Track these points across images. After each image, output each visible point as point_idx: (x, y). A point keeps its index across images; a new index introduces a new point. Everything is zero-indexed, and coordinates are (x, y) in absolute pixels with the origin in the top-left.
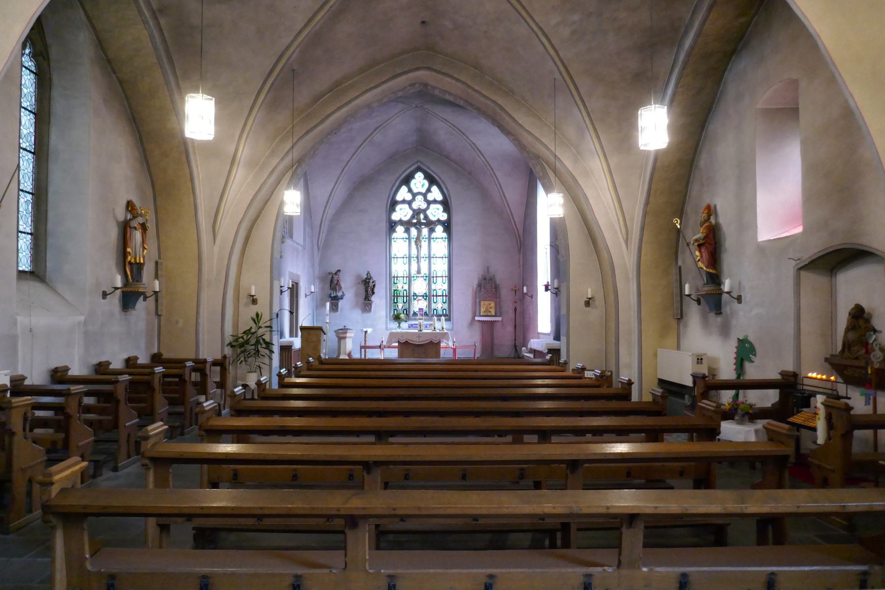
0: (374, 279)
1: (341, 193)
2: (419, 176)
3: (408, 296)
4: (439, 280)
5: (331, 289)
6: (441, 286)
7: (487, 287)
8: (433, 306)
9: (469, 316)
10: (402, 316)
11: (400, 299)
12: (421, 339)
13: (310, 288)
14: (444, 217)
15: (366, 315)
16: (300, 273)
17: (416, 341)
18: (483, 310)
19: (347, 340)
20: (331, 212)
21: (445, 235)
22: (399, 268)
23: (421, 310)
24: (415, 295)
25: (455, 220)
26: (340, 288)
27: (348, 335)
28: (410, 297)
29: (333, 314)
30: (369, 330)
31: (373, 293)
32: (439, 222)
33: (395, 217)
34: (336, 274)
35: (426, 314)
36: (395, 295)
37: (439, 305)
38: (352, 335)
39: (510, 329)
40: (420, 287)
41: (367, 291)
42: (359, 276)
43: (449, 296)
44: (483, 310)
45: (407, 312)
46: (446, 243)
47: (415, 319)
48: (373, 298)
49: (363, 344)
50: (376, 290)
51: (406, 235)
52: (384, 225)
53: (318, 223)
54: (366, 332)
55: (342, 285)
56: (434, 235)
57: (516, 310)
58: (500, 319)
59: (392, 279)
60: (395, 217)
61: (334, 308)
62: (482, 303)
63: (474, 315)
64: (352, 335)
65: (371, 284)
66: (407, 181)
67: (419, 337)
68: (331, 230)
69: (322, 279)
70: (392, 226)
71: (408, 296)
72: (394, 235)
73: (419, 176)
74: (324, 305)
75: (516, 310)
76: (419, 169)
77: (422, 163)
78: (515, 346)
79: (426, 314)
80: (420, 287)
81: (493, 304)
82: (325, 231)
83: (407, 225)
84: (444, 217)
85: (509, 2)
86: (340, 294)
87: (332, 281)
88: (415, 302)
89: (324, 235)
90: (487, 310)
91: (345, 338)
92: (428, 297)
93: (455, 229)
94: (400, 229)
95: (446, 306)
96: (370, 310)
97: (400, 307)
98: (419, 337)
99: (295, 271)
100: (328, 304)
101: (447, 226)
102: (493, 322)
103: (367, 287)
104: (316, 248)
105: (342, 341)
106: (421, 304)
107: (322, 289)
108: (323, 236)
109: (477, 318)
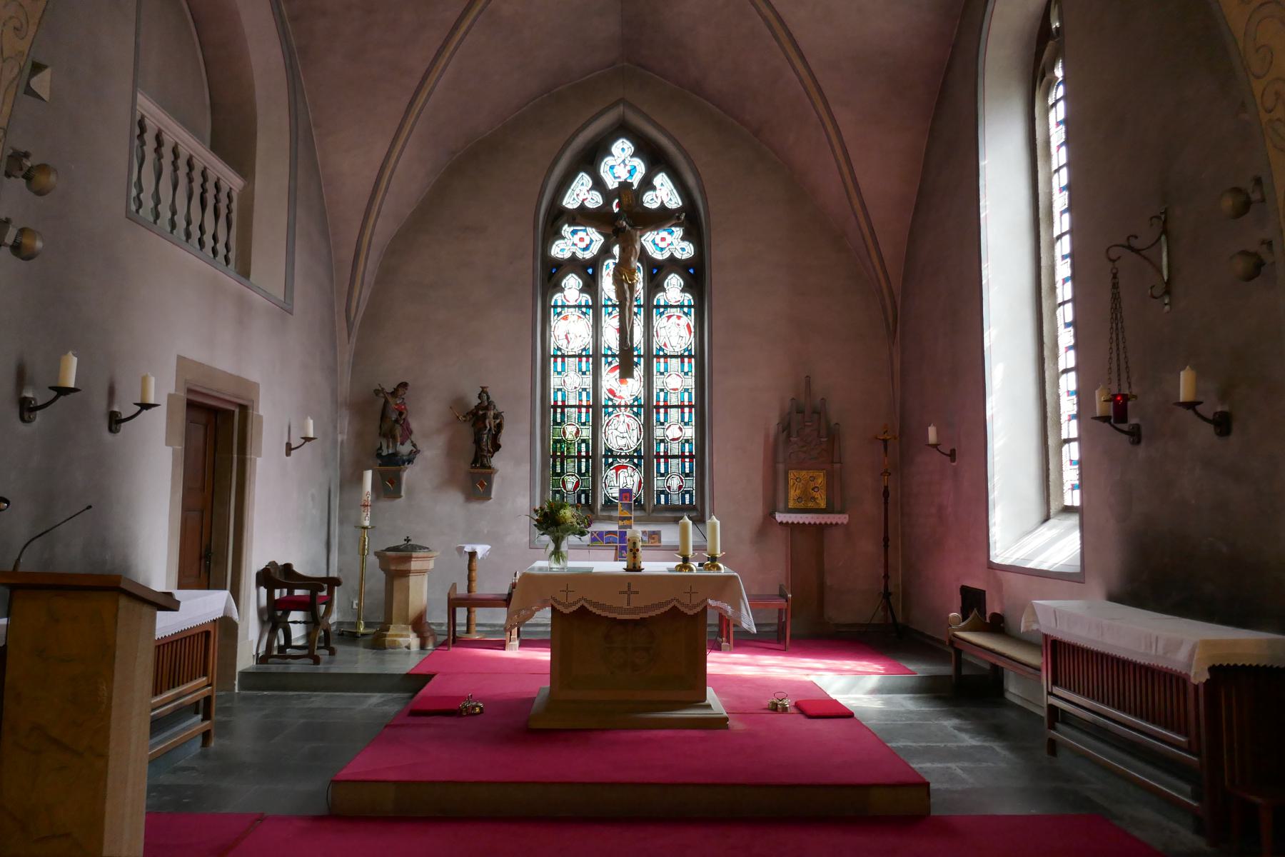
0: (500, 407)
1: (410, 178)
2: (622, 149)
3: (592, 457)
4: (674, 414)
5: (377, 438)
6: (677, 430)
7: (804, 434)
8: (658, 483)
9: (758, 511)
10: (568, 513)
11: (570, 466)
12: (637, 602)
13: (303, 427)
14: (685, 251)
15: (475, 506)
16: (253, 374)
17: (620, 607)
18: (793, 494)
19: (413, 580)
20: (383, 229)
21: (688, 298)
22: (569, 382)
23: (625, 492)
24: (609, 453)
25: (722, 252)
26: (408, 432)
27: (415, 565)
28: (598, 459)
29: (385, 504)
30: (481, 550)
31: (497, 447)
32: (672, 264)
33: (560, 250)
34: (394, 393)
35: (639, 505)
36: (556, 455)
37: (674, 481)
38: (431, 565)
39: (868, 546)
40: (621, 433)
41: (478, 441)
42: (458, 402)
43: (699, 457)
44: (793, 494)
45: (589, 504)
46: (691, 320)
47: (610, 519)
48: (496, 461)
49: (462, 590)
50: (504, 439)
51: (585, 298)
52: (527, 268)
53: (348, 254)
54: (472, 555)
55: (414, 425)
56: (660, 298)
57: (886, 493)
58: (842, 519)
59: (552, 411)
60: (560, 250)
61: (389, 486)
62: (791, 475)
63: (770, 515)
64: (431, 565)
65: (490, 422)
66: (590, 159)
67: (629, 592)
68: (387, 274)
69: (358, 408)
70: (552, 273)
71: (592, 457)
72: (558, 298)
73: (622, 149)
74: (360, 479)
75: (886, 493)
76: (622, 129)
77: (632, 106)
78: (887, 595)
79: (639, 505)
80: (621, 433)
81: (820, 480)
82: (370, 278)
83: (588, 271)
84: (685, 251)
85: (753, 4)
86: (405, 449)
87: (384, 416)
88: (612, 473)
89: (366, 293)
90: (805, 495)
91: (406, 574)
92: (645, 457)
93: (717, 278)
94: (572, 283)
95: (690, 484)
96: (486, 495)
97: (570, 486)
98: (629, 592)
99: (197, 354)
100: (368, 475)
101: (695, 275)
102: (821, 528)
103: (479, 432)
104: (341, 323)
105: (397, 584)
106: (629, 479)
107: (359, 436)
108: (363, 294)
109: (780, 517)
